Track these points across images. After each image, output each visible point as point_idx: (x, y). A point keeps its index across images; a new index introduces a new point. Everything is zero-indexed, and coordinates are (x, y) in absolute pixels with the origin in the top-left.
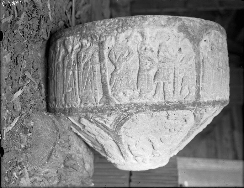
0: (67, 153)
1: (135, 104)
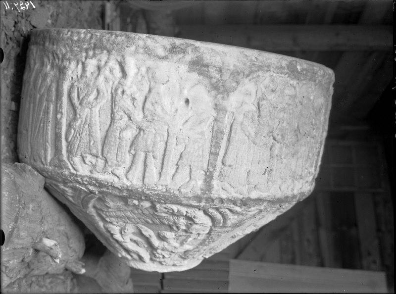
1: (96, 180)
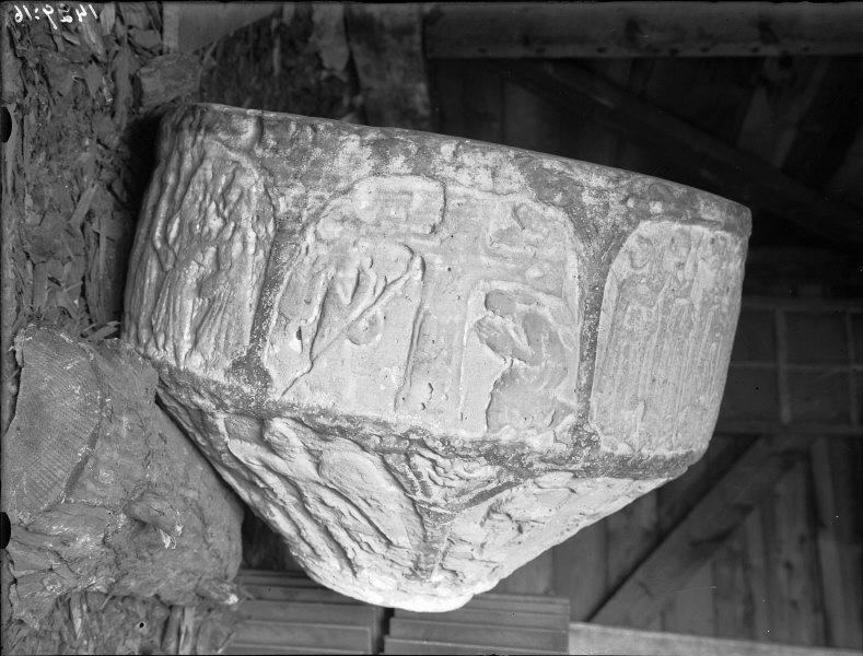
0: (138, 474)
